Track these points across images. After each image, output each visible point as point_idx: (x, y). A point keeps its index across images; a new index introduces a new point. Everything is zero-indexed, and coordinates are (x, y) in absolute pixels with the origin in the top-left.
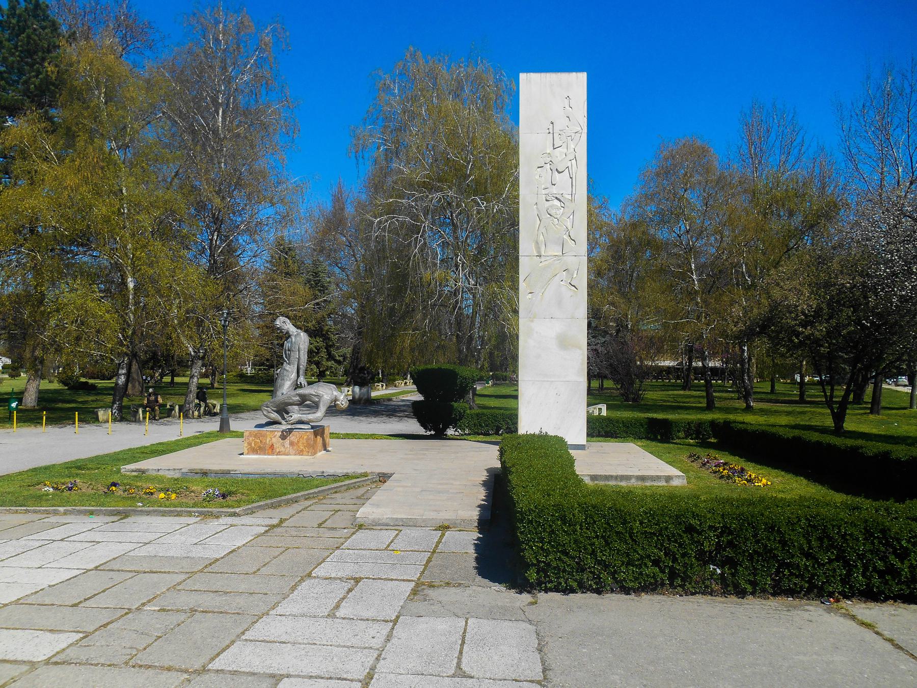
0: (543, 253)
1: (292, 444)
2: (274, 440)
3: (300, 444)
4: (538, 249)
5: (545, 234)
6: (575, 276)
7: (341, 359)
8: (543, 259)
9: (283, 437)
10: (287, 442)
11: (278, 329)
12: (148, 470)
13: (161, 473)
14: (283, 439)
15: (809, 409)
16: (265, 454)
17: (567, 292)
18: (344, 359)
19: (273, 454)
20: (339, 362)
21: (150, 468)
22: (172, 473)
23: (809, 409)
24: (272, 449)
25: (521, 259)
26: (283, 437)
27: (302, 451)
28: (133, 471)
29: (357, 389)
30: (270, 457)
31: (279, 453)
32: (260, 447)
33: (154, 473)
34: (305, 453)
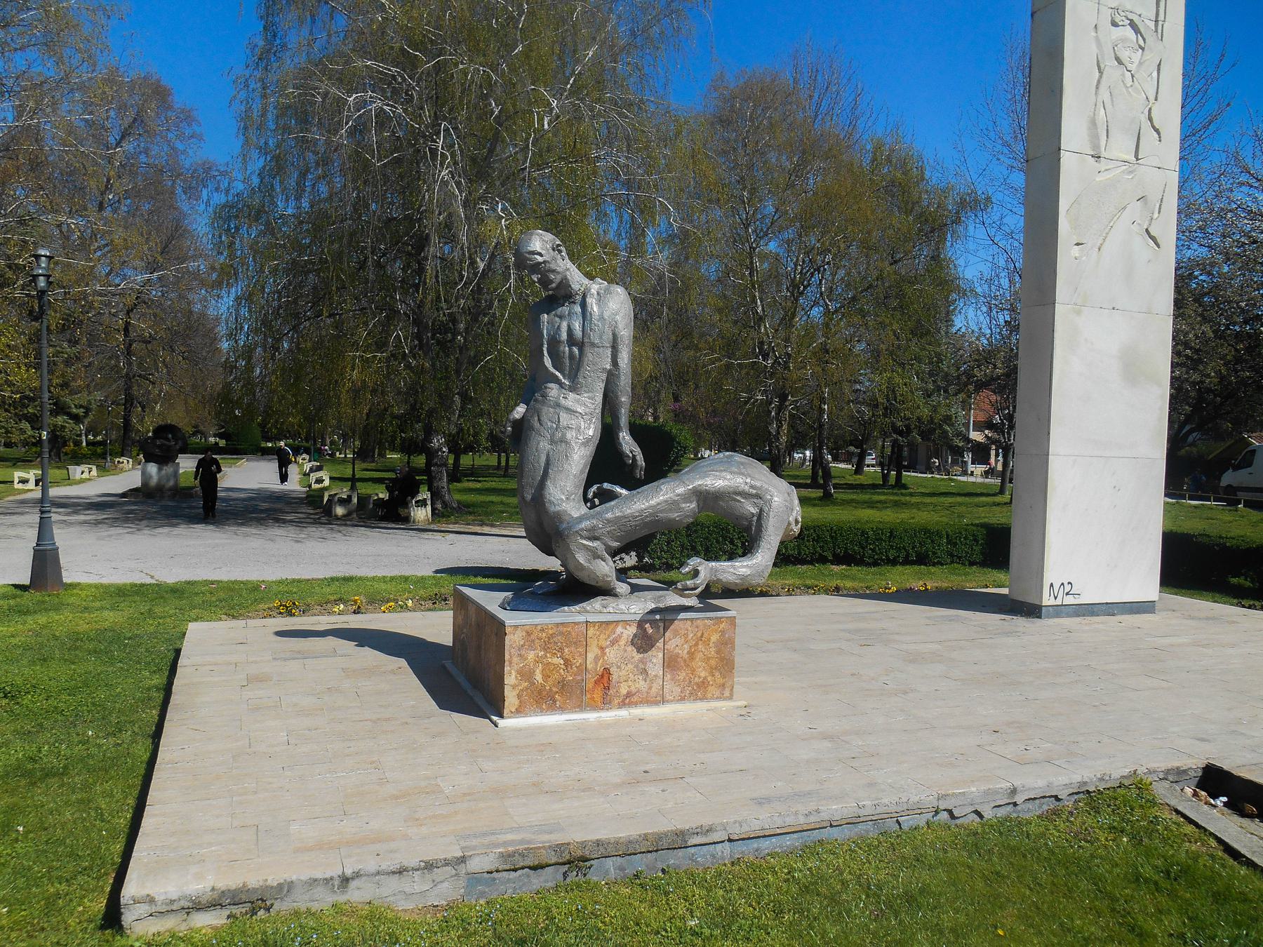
0: (1103, 154)
1: (671, 663)
2: (612, 655)
3: (698, 663)
4: (1094, 139)
5: (1108, 105)
6: (1156, 215)
7: (81, 411)
8: (1103, 165)
9: (643, 642)
10: (655, 658)
11: (536, 268)
12: (286, 888)
13: (357, 894)
14: (642, 650)
15: (883, 498)
16: (581, 707)
17: (1142, 247)
18: (86, 414)
19: (606, 703)
20: (76, 419)
21: (297, 872)
22: (417, 884)
23: (883, 498)
24: (602, 688)
25: (1065, 157)
26: (643, 642)
27: (703, 685)
28: (197, 906)
29: (152, 468)
30: (592, 716)
31: (628, 700)
32: (563, 685)
33: (323, 900)
34: (712, 690)
